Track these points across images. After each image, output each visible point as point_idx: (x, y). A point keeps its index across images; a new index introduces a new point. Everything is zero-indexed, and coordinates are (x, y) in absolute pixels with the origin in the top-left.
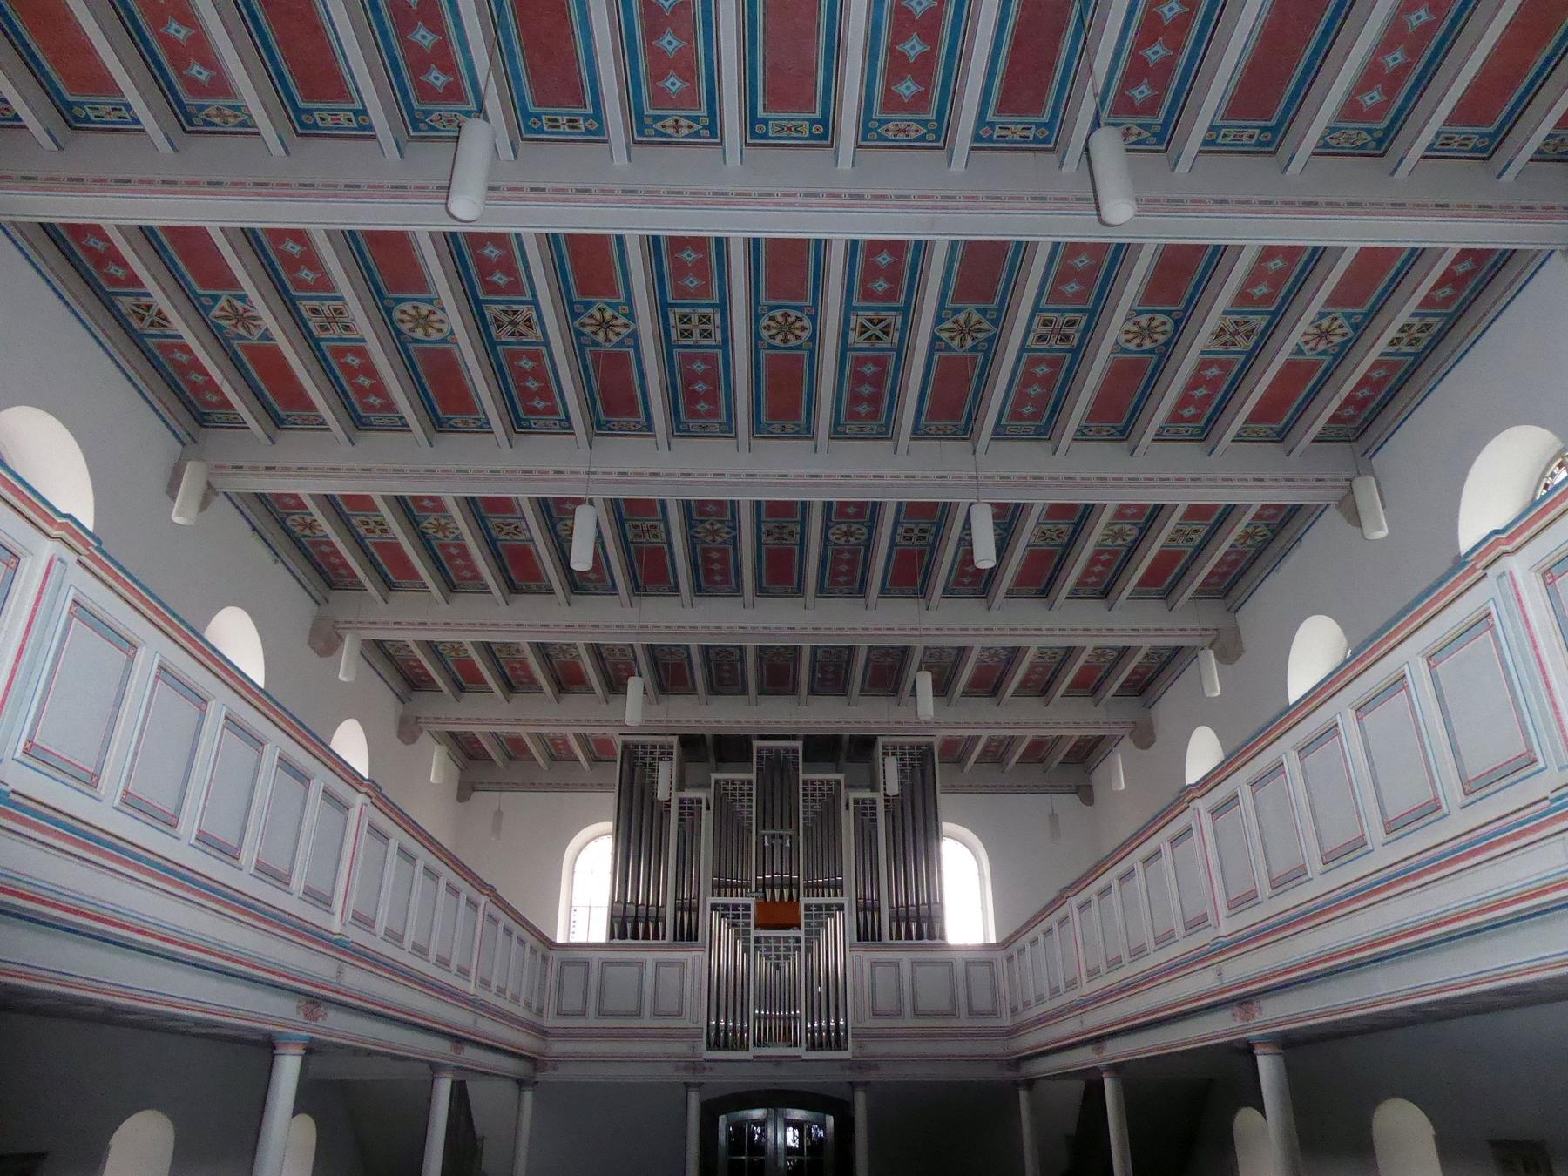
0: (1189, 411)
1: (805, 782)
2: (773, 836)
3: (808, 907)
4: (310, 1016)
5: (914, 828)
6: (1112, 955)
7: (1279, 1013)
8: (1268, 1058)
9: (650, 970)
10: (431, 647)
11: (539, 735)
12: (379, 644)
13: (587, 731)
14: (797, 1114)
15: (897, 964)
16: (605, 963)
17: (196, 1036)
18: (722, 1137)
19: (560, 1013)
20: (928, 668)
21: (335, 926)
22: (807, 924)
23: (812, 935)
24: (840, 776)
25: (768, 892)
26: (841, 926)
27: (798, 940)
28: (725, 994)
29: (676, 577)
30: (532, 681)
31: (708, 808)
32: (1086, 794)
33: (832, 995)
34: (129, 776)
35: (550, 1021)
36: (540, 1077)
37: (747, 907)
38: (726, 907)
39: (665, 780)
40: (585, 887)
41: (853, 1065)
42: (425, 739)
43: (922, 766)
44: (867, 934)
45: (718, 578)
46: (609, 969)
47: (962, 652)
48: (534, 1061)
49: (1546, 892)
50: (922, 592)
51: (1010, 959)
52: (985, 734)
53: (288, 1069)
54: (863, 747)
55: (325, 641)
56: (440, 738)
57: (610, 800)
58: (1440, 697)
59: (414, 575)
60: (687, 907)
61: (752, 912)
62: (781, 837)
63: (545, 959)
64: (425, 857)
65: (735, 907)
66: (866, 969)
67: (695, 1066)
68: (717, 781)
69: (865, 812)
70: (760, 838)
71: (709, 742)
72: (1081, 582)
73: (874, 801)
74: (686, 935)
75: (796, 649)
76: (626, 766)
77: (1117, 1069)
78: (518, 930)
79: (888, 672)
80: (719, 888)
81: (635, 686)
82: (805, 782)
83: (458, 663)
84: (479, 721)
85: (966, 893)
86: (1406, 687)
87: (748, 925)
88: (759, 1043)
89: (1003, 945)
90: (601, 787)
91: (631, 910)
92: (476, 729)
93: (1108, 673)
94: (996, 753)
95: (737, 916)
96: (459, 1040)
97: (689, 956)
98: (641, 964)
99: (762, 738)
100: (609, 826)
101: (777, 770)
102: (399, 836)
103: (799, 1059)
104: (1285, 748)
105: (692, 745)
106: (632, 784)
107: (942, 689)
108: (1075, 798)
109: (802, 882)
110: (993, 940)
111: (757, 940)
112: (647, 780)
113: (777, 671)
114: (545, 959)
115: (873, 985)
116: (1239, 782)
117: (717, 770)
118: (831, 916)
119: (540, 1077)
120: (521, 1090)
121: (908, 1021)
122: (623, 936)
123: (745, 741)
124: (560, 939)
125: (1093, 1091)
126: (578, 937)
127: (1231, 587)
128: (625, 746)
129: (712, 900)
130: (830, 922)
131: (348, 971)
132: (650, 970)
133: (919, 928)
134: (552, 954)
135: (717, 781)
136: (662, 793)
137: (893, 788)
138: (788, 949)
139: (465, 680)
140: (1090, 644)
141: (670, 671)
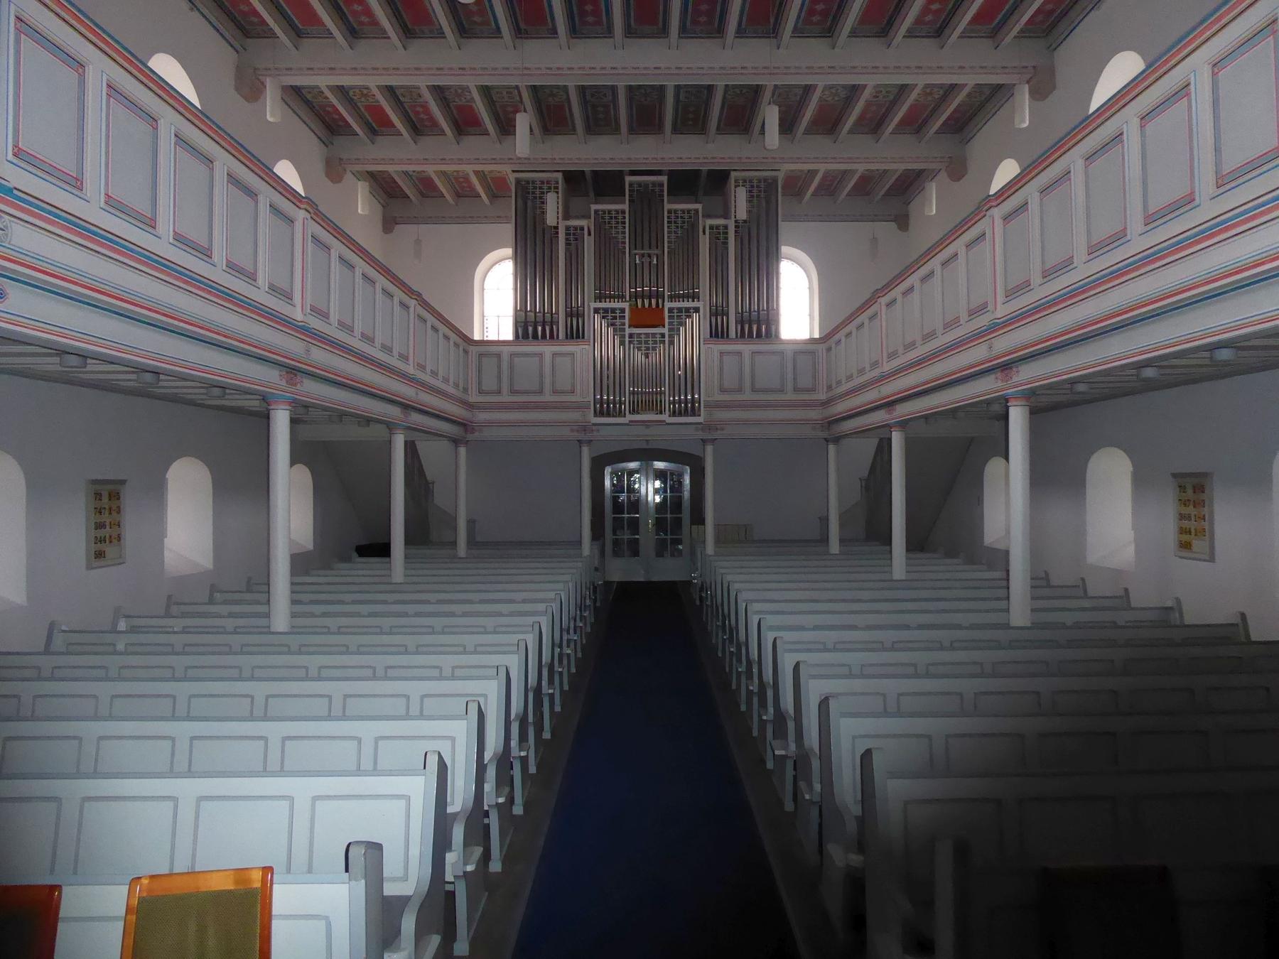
0: (929, 18)
1: (669, 212)
2: (643, 255)
3: (671, 310)
4: (291, 382)
5: (758, 265)
6: (909, 340)
7: (1028, 375)
8: (1018, 409)
9: (548, 359)
10: (341, 91)
11: (444, 173)
12: (297, 91)
13: (487, 168)
14: (660, 465)
16: (512, 355)
17: (209, 407)
18: (607, 483)
19: (481, 392)
20: (774, 103)
21: (298, 316)
22: (670, 324)
23: (674, 331)
24: (699, 206)
25: (639, 302)
26: (696, 326)
27: (663, 335)
28: (606, 378)
29: (553, 19)
30: (435, 124)
31: (589, 234)
32: (902, 221)
33: (691, 378)
34: (107, 184)
35: (474, 398)
36: (470, 437)
37: (623, 310)
38: (606, 310)
39: (552, 214)
40: (495, 299)
41: (708, 427)
42: (349, 177)
43: (766, 194)
44: (718, 333)
45: (590, 19)
47: (808, 90)
48: (464, 425)
49: (1263, 263)
50: (773, 32)
51: (829, 349)
52: (822, 168)
53: (281, 421)
54: (718, 180)
55: (250, 88)
56: (359, 176)
57: (508, 230)
58: (1216, 103)
59: (319, 22)
60: (575, 314)
61: (627, 314)
62: (649, 256)
63: (466, 352)
64: (361, 265)
65: (613, 310)
66: (716, 354)
67: (585, 428)
68: (596, 212)
69: (718, 237)
70: (632, 257)
71: (588, 176)
72: (918, 21)
73: (726, 227)
74: (576, 334)
75: (662, 89)
76: (520, 202)
77: (903, 425)
78: (443, 329)
79: (740, 112)
80: (599, 298)
81: (523, 122)
82: (669, 212)
83: (368, 108)
84: (392, 161)
85: (797, 301)
86: (1188, 94)
89: (824, 339)
90: (499, 219)
92: (391, 169)
93: (934, 110)
94: (830, 186)
95: (615, 318)
96: (406, 407)
97: (579, 349)
98: (541, 355)
99: (633, 173)
100: (509, 251)
101: (646, 201)
102: (337, 247)
103: (665, 426)
104: (1074, 159)
105: (574, 180)
106: (525, 217)
107: (787, 126)
108: (893, 225)
109: (667, 293)
110: (817, 336)
112: (538, 212)
113: (646, 111)
114: (466, 352)
115: (721, 369)
116: (1031, 191)
117: (596, 203)
118: (689, 317)
119: (470, 437)
120: (456, 447)
121: (748, 396)
122: (526, 336)
123: (619, 175)
124: (477, 337)
125: (884, 447)
126: (492, 336)
127: (1053, 26)
128: (518, 181)
129: (594, 305)
131: (314, 350)
132: (548, 359)
133: (759, 330)
134: (471, 348)
135: (596, 212)
136: (551, 220)
137: (742, 214)
138: (655, 342)
139: (377, 125)
140: (921, 81)
141: (553, 114)
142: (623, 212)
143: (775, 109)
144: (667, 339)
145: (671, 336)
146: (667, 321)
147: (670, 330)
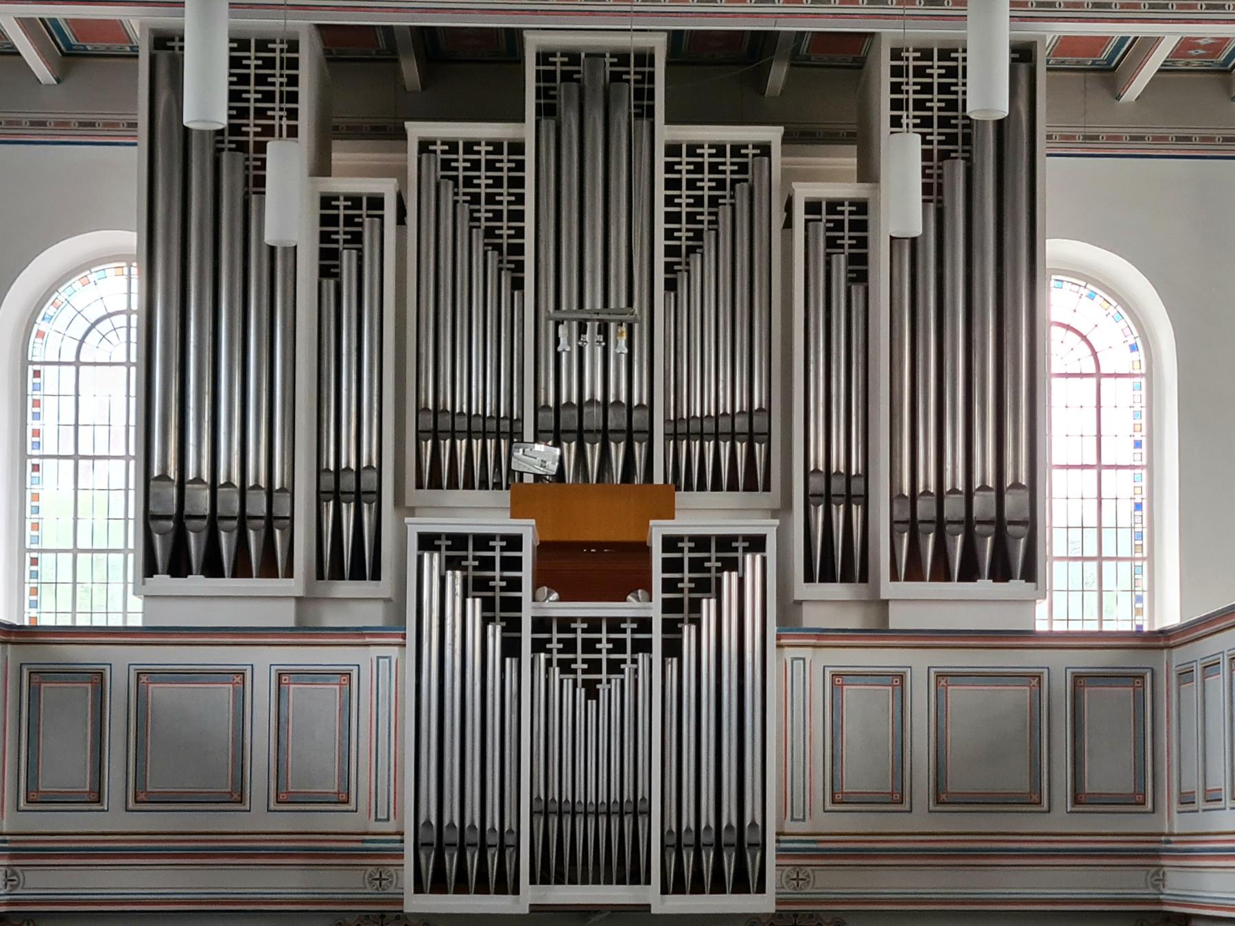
1: (673, 149)
15: (898, 679)
22: (668, 586)
23: (680, 611)
27: (644, 624)
46: (157, 691)
61: (527, 555)
87: (516, 584)
88: (542, 876)
90: (88, 131)
91: (200, 501)
100: (130, 239)
111: (541, 624)
118: (732, 565)
121: (921, 819)
130: (729, 580)
138: (619, 646)
142: (517, 147)
143: (914, 144)
144: (657, 636)
145: (671, 627)
146: (657, 576)
147: (668, 606)
